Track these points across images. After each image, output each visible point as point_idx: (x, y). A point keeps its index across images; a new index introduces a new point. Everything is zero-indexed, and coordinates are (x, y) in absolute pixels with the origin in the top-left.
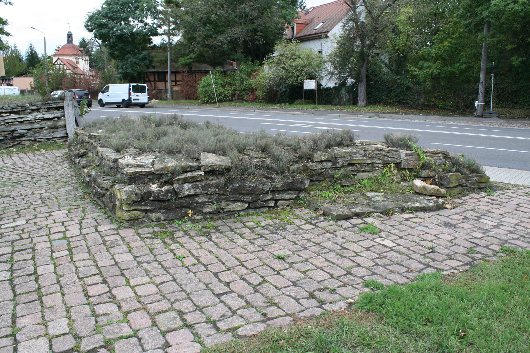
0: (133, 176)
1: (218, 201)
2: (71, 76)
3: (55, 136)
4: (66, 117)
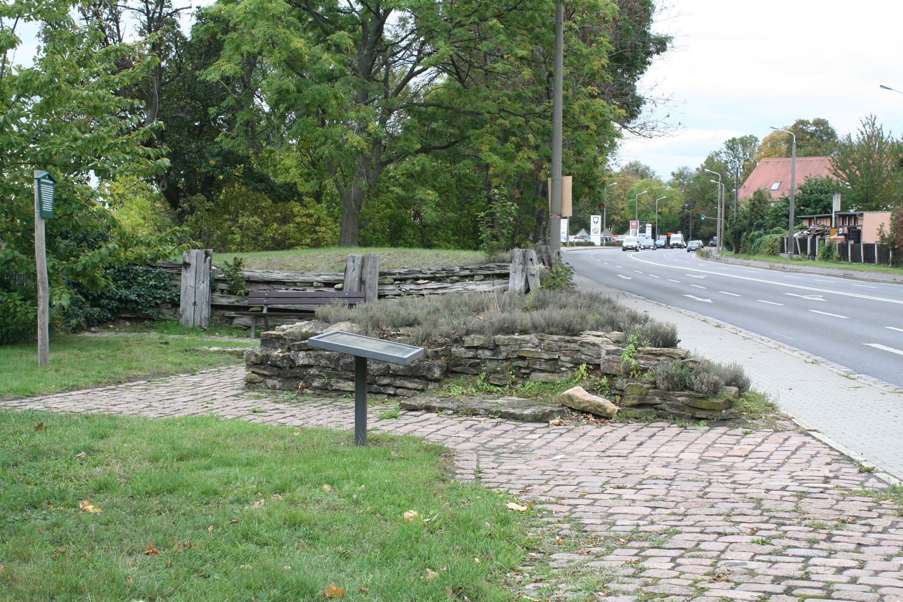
1: (330, 376)
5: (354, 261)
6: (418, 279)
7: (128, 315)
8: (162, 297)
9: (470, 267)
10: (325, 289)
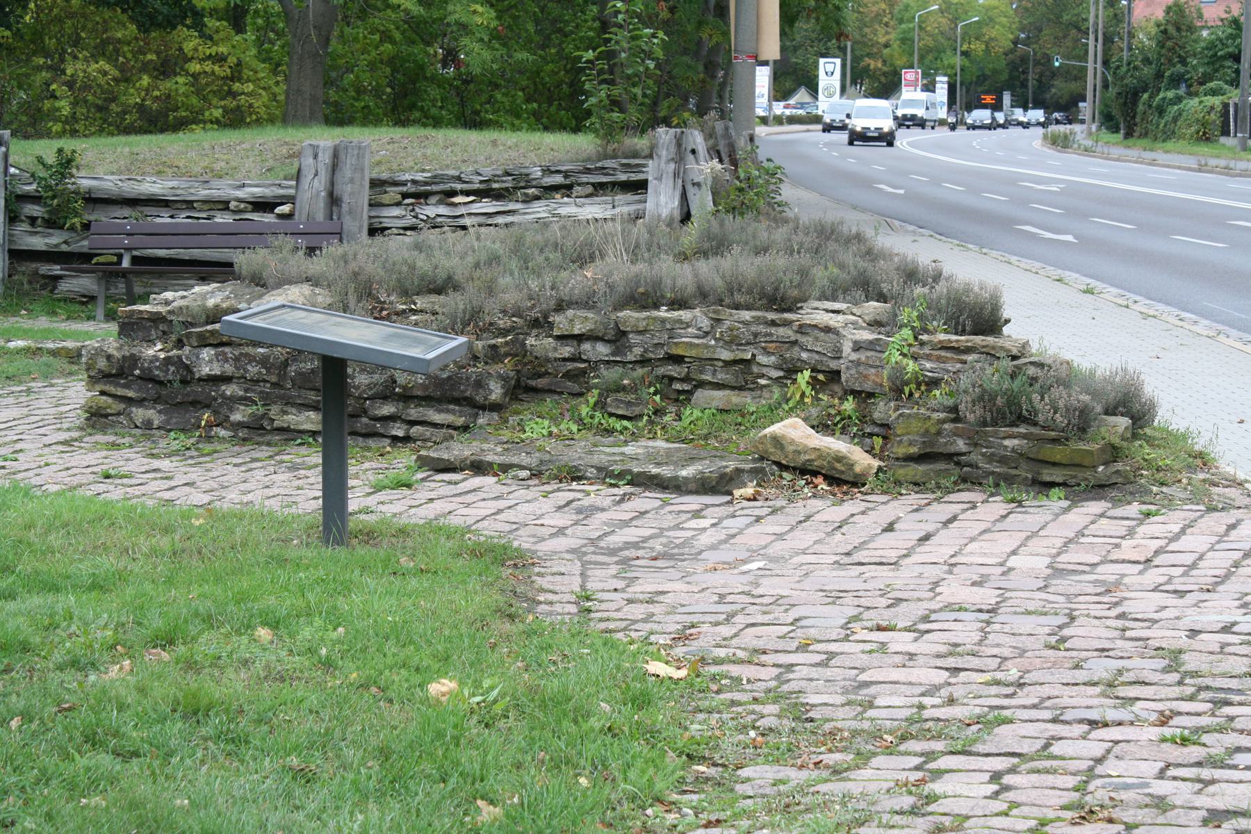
0: (126, 320)
1: (267, 400)
5: (316, 156)
9: (563, 168)
10: (256, 217)
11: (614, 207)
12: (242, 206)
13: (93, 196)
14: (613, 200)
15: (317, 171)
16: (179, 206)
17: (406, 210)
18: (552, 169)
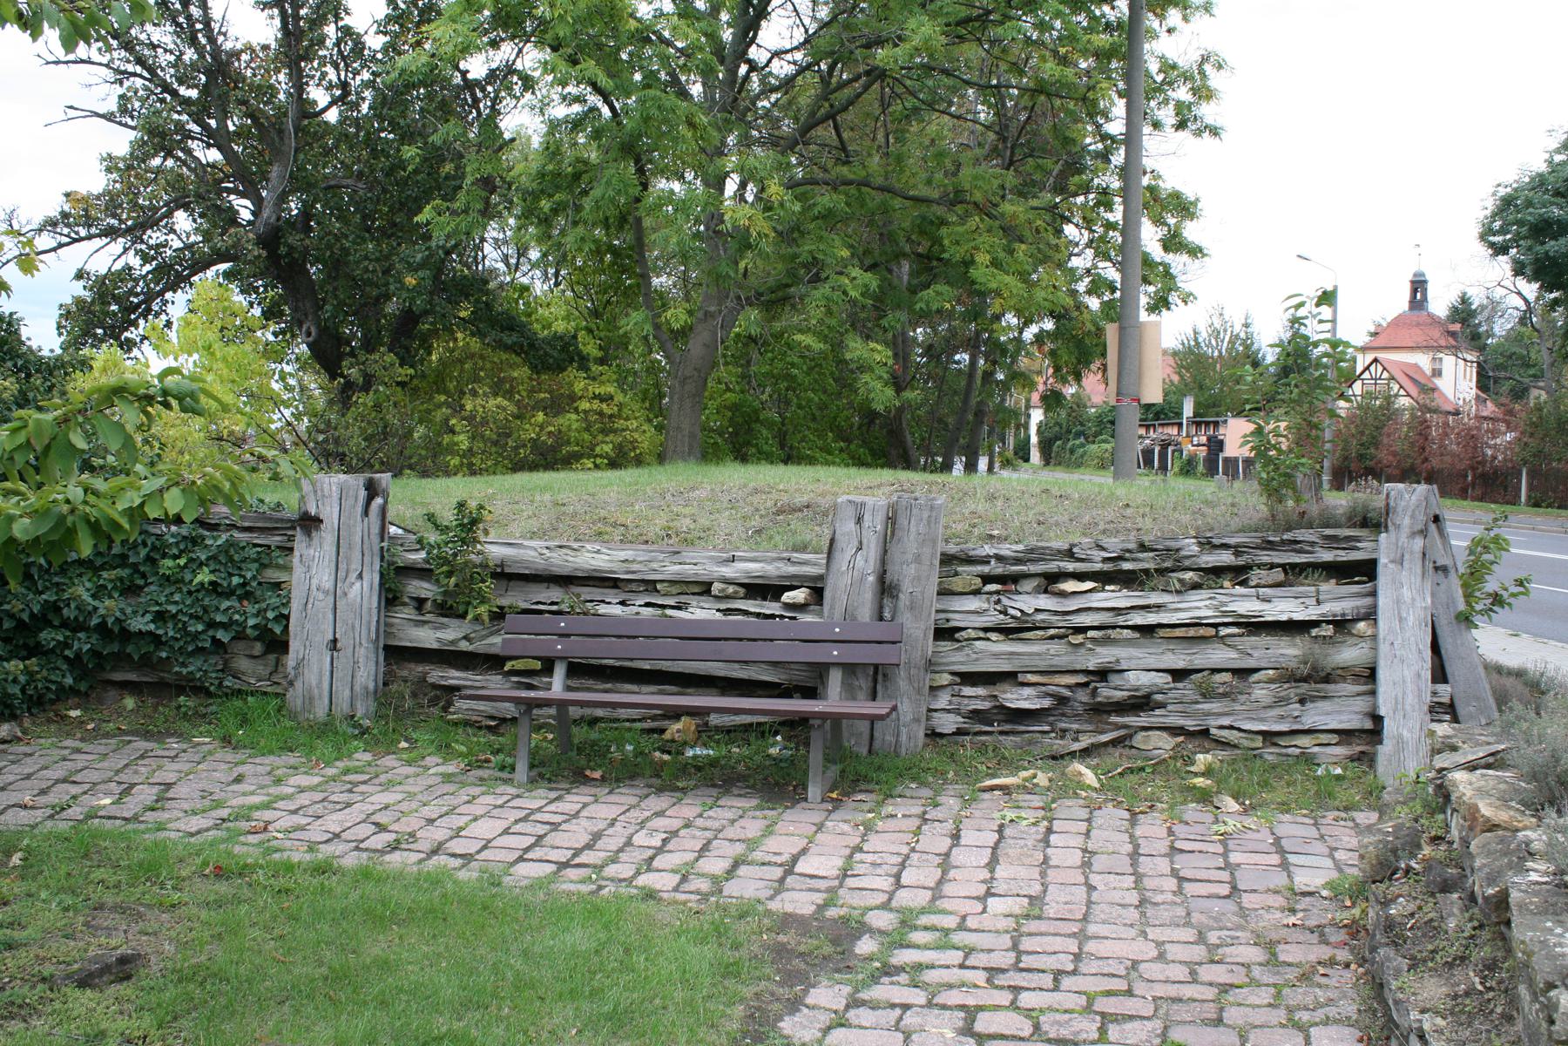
2: (1413, 416)
3: (1308, 722)
4: (1381, 623)
5: (859, 520)
6: (1053, 578)
7: (132, 677)
8: (232, 622)
9: (1232, 541)
10: (752, 606)
11: (1319, 602)
12: (731, 589)
13: (507, 570)
14: (1318, 592)
15: (861, 543)
16: (633, 587)
17: (988, 601)
18: (1216, 541)
